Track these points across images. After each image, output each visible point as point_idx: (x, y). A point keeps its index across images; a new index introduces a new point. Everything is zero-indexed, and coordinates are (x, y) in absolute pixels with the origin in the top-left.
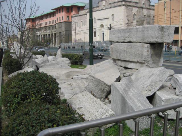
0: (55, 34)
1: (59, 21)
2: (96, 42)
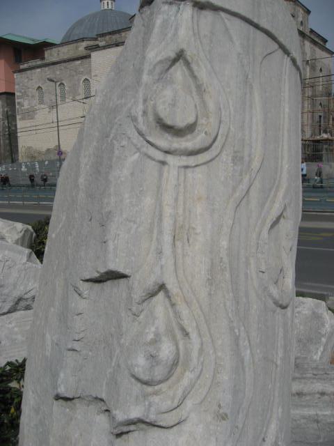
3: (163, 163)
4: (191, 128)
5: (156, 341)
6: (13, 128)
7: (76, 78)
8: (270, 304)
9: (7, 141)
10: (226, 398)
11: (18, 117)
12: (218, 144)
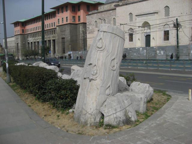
0: (54, 41)
1: (61, 24)
2: (141, 49)
3: (97, 52)
4: (101, 48)
5: (94, 70)
6: (85, 37)
7: (110, 18)
8: (111, 70)
9: (83, 42)
10: (102, 79)
11: (87, 32)
12: (105, 50)
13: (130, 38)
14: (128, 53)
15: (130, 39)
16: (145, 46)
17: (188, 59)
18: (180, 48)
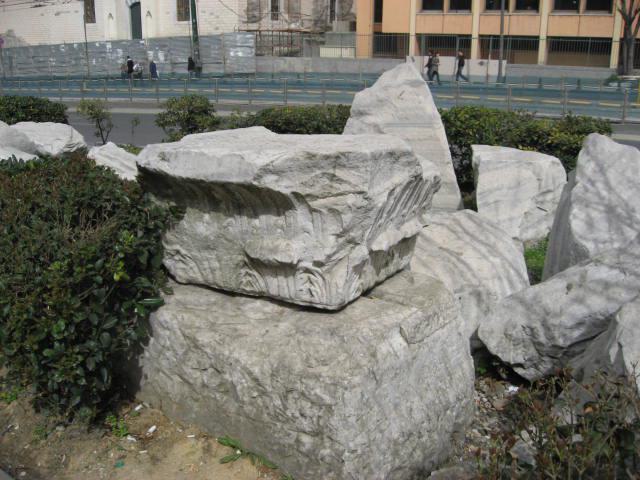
2: (109, 46)
13: (86, 10)
14: (76, 59)
15: (179, 13)
16: (130, 38)
17: (222, 71)
18: (202, 43)
